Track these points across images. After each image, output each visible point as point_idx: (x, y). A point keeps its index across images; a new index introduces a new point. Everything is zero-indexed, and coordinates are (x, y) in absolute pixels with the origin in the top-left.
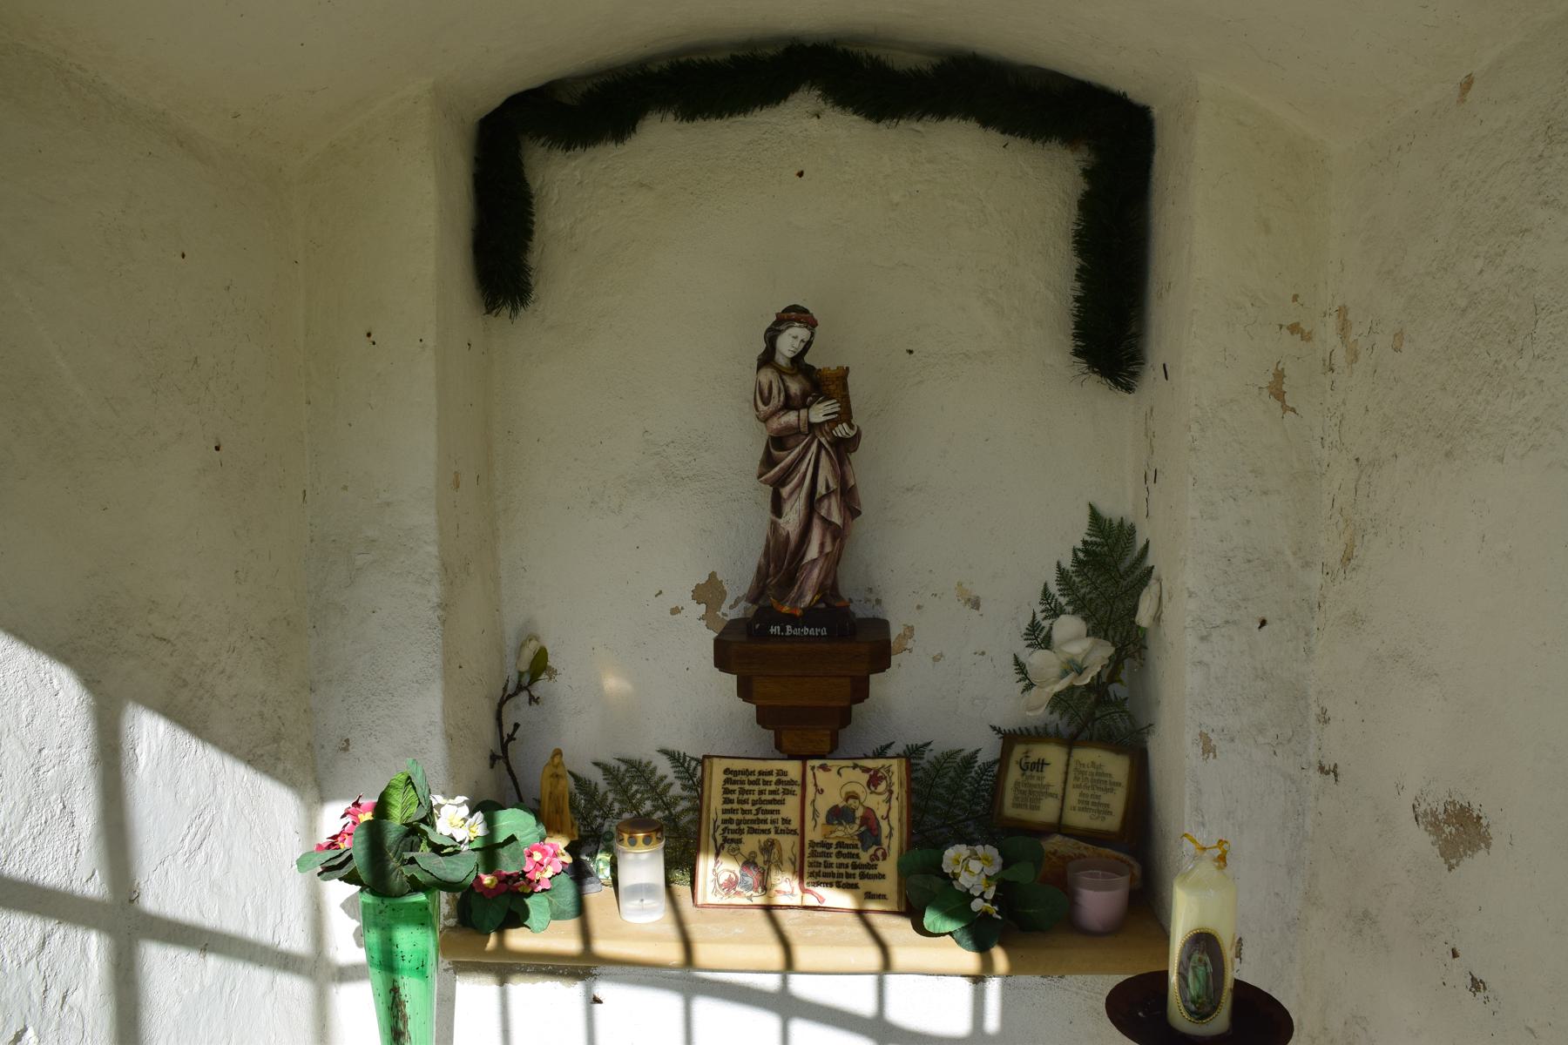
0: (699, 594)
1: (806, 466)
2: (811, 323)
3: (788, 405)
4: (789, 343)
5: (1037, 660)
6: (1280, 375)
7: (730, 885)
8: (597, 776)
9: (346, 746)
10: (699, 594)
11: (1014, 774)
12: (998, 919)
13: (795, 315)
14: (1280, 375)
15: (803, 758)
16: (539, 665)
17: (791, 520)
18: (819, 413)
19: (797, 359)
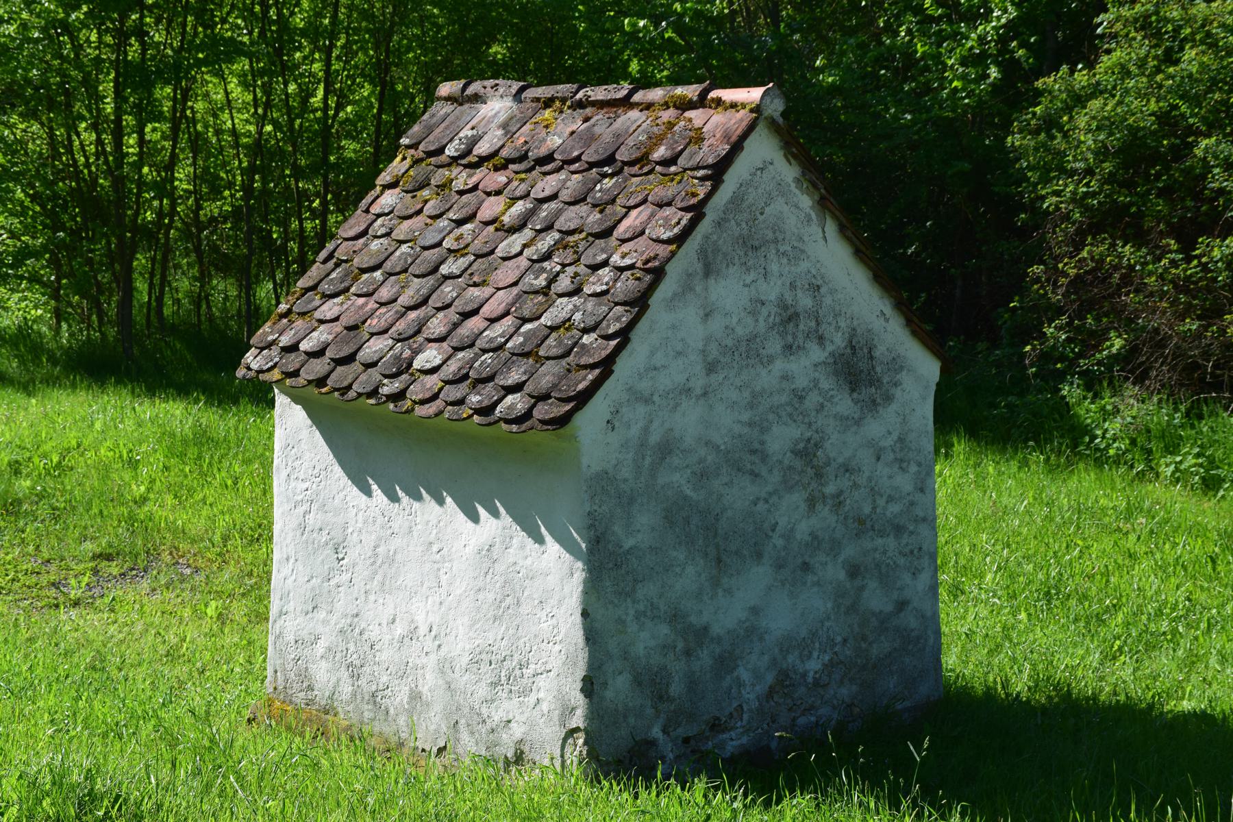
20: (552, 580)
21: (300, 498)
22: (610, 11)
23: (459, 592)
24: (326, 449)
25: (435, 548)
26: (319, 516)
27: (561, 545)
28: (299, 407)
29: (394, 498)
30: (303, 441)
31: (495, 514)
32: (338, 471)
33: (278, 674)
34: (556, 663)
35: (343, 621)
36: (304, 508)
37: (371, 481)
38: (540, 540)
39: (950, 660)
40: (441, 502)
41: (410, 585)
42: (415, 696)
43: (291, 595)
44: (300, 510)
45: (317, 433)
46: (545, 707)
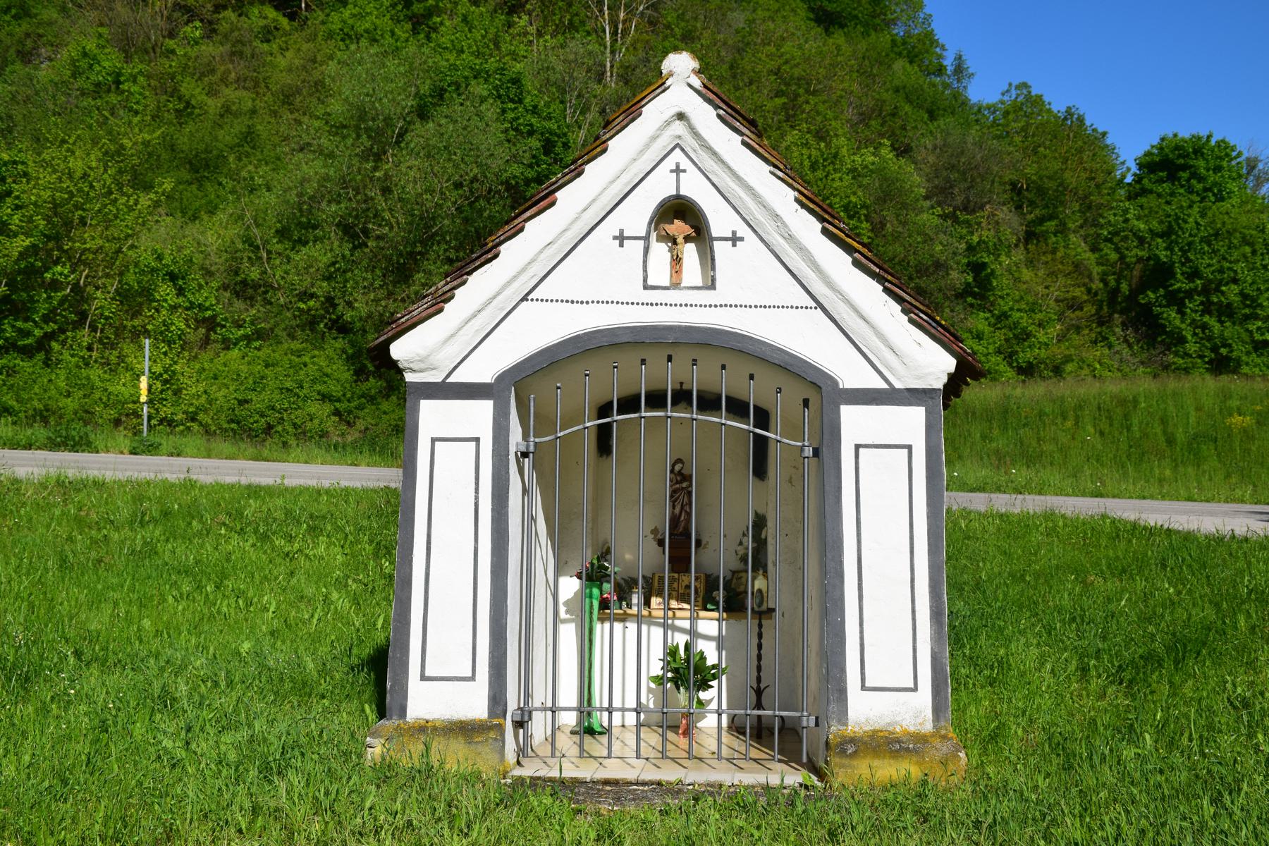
0: (652, 532)
1: (681, 498)
2: (683, 463)
3: (677, 482)
4: (677, 468)
5: (740, 548)
6: (791, 478)
7: (660, 604)
8: (622, 582)
9: (566, 563)
10: (652, 532)
11: (735, 581)
12: (728, 680)
13: (679, 461)
14: (791, 478)
15: (679, 573)
16: (608, 551)
17: (677, 510)
18: (684, 485)
19: (680, 471)
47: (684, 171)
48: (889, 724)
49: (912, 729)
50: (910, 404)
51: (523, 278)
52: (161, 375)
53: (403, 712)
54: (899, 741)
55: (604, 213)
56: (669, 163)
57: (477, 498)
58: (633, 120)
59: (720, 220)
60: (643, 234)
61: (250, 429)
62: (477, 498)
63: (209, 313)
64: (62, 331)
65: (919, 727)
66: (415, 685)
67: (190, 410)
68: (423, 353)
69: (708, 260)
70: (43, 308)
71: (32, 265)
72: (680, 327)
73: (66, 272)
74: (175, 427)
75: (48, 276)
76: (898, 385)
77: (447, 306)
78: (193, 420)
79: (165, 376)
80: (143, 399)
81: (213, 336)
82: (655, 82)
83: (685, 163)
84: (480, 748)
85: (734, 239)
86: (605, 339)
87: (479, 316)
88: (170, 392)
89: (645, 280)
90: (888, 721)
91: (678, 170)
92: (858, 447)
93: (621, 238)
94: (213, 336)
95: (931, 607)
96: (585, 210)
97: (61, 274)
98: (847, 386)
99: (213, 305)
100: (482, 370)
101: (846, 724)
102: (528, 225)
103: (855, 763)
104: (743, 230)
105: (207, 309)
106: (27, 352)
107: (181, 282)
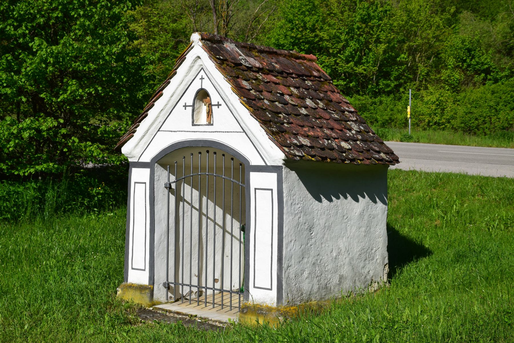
20: (380, 216)
21: (296, 212)
22: (60, 59)
23: (353, 231)
24: (305, 188)
25: (345, 217)
26: (304, 218)
27: (312, 195)
28: (294, 172)
29: (331, 200)
30: (296, 187)
31: (364, 197)
32: (310, 196)
33: (289, 295)
34: (381, 245)
35: (314, 259)
36: (298, 216)
37: (322, 196)
38: (375, 202)
39: (133, 169)
40: (346, 198)
41: (337, 235)
42: (341, 278)
43: (293, 257)
44: (297, 217)
45: (301, 182)
46: (378, 261)
47: (204, 79)
48: (262, 302)
49: (270, 305)
50: (272, 172)
51: (156, 123)
52: (435, 102)
53: (127, 281)
54: (262, 310)
55: (180, 97)
56: (199, 76)
57: (146, 204)
58: (183, 61)
59: (215, 98)
60: (191, 104)
61: (470, 126)
62: (146, 204)
63: (486, 66)
64: (405, 83)
65: (272, 305)
66: (131, 272)
67: (447, 118)
68: (129, 151)
69: (210, 113)
70: (395, 74)
71: (391, 55)
72: (203, 140)
73: (405, 57)
74: (440, 126)
75: (398, 59)
76: (269, 164)
77: (135, 134)
78: (449, 122)
79: (437, 102)
80: (409, 116)
81: (489, 77)
82: (189, 46)
83: (205, 76)
84: (144, 295)
85: (218, 105)
86: (181, 145)
87: (144, 138)
88: (439, 110)
89: (193, 122)
90: (262, 301)
91: (202, 79)
92: (256, 189)
93: (185, 106)
94: (489, 77)
95: (278, 256)
96: (172, 96)
97: (403, 58)
98: (253, 164)
99: (488, 62)
100: (147, 158)
101: (248, 301)
102: (156, 103)
103: (246, 316)
104: (221, 102)
105: (486, 64)
106: (388, 93)
107: (473, 53)
